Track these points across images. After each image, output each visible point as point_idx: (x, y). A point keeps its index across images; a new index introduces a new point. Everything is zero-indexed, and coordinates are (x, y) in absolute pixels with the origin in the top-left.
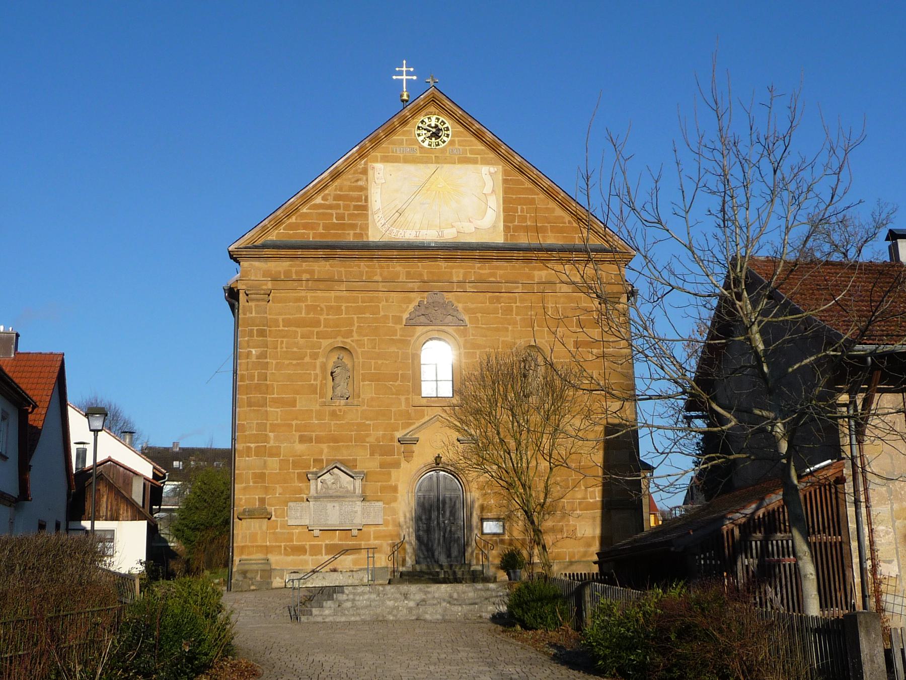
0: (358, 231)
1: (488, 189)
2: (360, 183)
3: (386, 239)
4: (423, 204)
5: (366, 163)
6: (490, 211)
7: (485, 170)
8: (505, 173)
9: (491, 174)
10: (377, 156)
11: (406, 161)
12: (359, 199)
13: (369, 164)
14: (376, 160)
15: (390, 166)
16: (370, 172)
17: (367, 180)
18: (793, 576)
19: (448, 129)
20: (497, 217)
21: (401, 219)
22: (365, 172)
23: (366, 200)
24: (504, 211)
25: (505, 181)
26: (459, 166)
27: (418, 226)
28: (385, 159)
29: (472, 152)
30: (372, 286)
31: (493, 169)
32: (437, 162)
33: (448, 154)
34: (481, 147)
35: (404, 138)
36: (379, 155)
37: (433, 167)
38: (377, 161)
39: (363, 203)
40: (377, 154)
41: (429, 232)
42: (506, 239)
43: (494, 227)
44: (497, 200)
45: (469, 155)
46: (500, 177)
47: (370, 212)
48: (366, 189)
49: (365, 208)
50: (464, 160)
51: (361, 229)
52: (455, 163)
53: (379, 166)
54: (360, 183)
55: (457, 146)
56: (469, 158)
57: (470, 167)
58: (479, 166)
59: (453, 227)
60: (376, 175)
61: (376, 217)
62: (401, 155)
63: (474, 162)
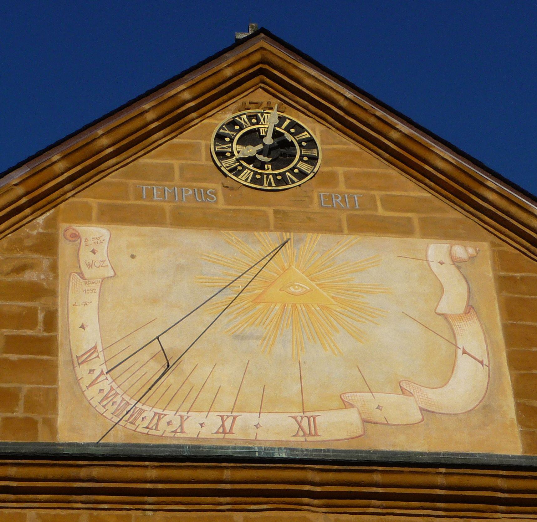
0: (19, 413)
1: (454, 298)
2: (29, 276)
3: (118, 437)
4: (241, 337)
5: (51, 224)
6: (464, 362)
7: (437, 251)
8: (501, 260)
9: (457, 263)
10: (88, 208)
11: (181, 220)
12: (27, 319)
13: (63, 226)
14: (86, 218)
15: (129, 234)
16: (65, 249)
17: (54, 268)
18: (267, 88)
19: (311, 142)
20: (493, 378)
21: (171, 378)
22: (48, 245)
23: (51, 321)
24: (514, 361)
25: (504, 283)
26: (355, 238)
27: (227, 400)
28: (114, 215)
29: (388, 203)
30: (187, 405)
31: (461, 251)
32: (281, 227)
33: (315, 206)
34: (414, 191)
35: (176, 163)
36: (94, 202)
37: (270, 239)
38: (86, 219)
39: (39, 331)
40: (89, 198)
41: (266, 419)
42: (527, 446)
43: (486, 408)
44: (487, 333)
45: (381, 211)
46: (487, 271)
47: (62, 357)
48: (52, 293)
49: (47, 345)
50: (366, 224)
51: (30, 406)
52: (339, 231)
53: (95, 233)
54: (29, 276)
55: (342, 187)
56: (384, 219)
57: (391, 243)
58: (417, 242)
59: (346, 405)
60: (85, 256)
61: (82, 371)
62: (167, 207)
63: (403, 229)
